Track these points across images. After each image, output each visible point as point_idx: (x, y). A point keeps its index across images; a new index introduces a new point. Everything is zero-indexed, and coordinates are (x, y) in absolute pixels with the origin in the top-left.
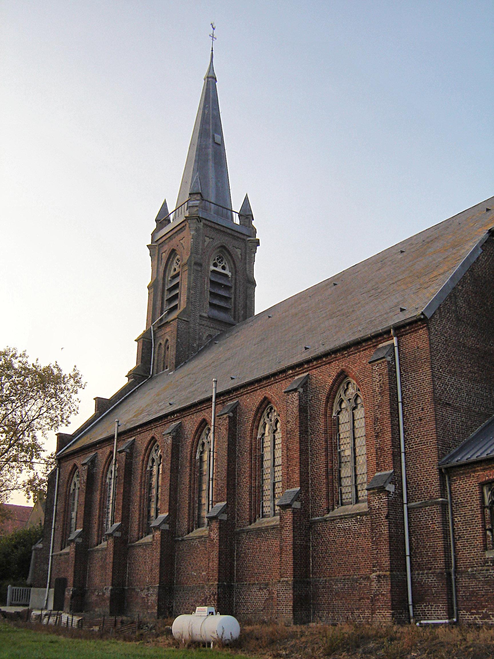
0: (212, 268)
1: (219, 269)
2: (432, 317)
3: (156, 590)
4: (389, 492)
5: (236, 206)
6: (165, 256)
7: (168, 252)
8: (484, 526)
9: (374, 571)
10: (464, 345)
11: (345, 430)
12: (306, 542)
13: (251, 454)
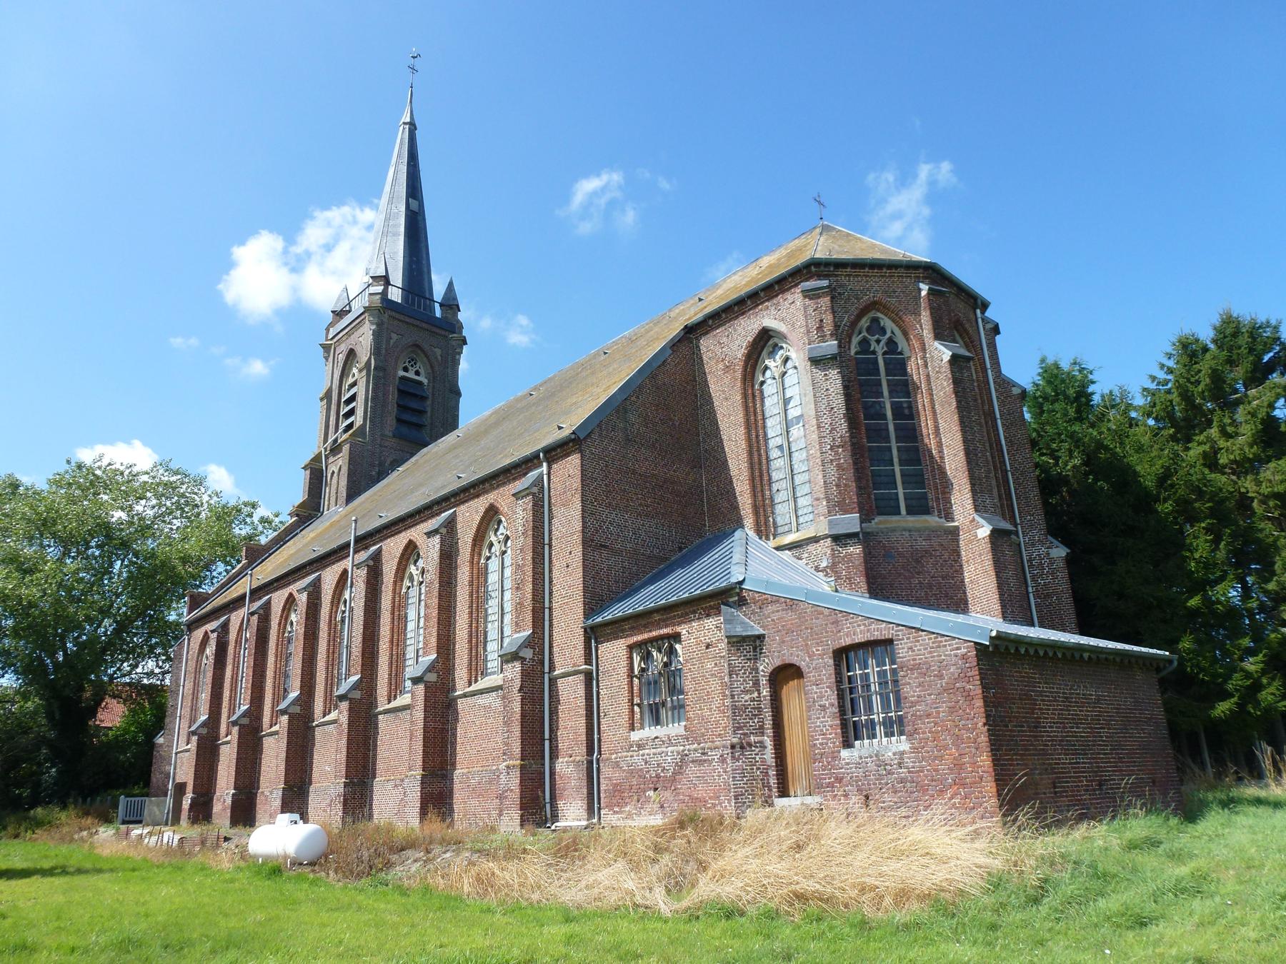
0: (401, 373)
1: (411, 375)
2: (589, 435)
3: (280, 793)
4: (524, 659)
5: (439, 291)
6: (342, 358)
7: (345, 353)
8: (631, 700)
9: (505, 760)
10: (634, 472)
11: (493, 578)
12: (443, 724)
13: (393, 614)
